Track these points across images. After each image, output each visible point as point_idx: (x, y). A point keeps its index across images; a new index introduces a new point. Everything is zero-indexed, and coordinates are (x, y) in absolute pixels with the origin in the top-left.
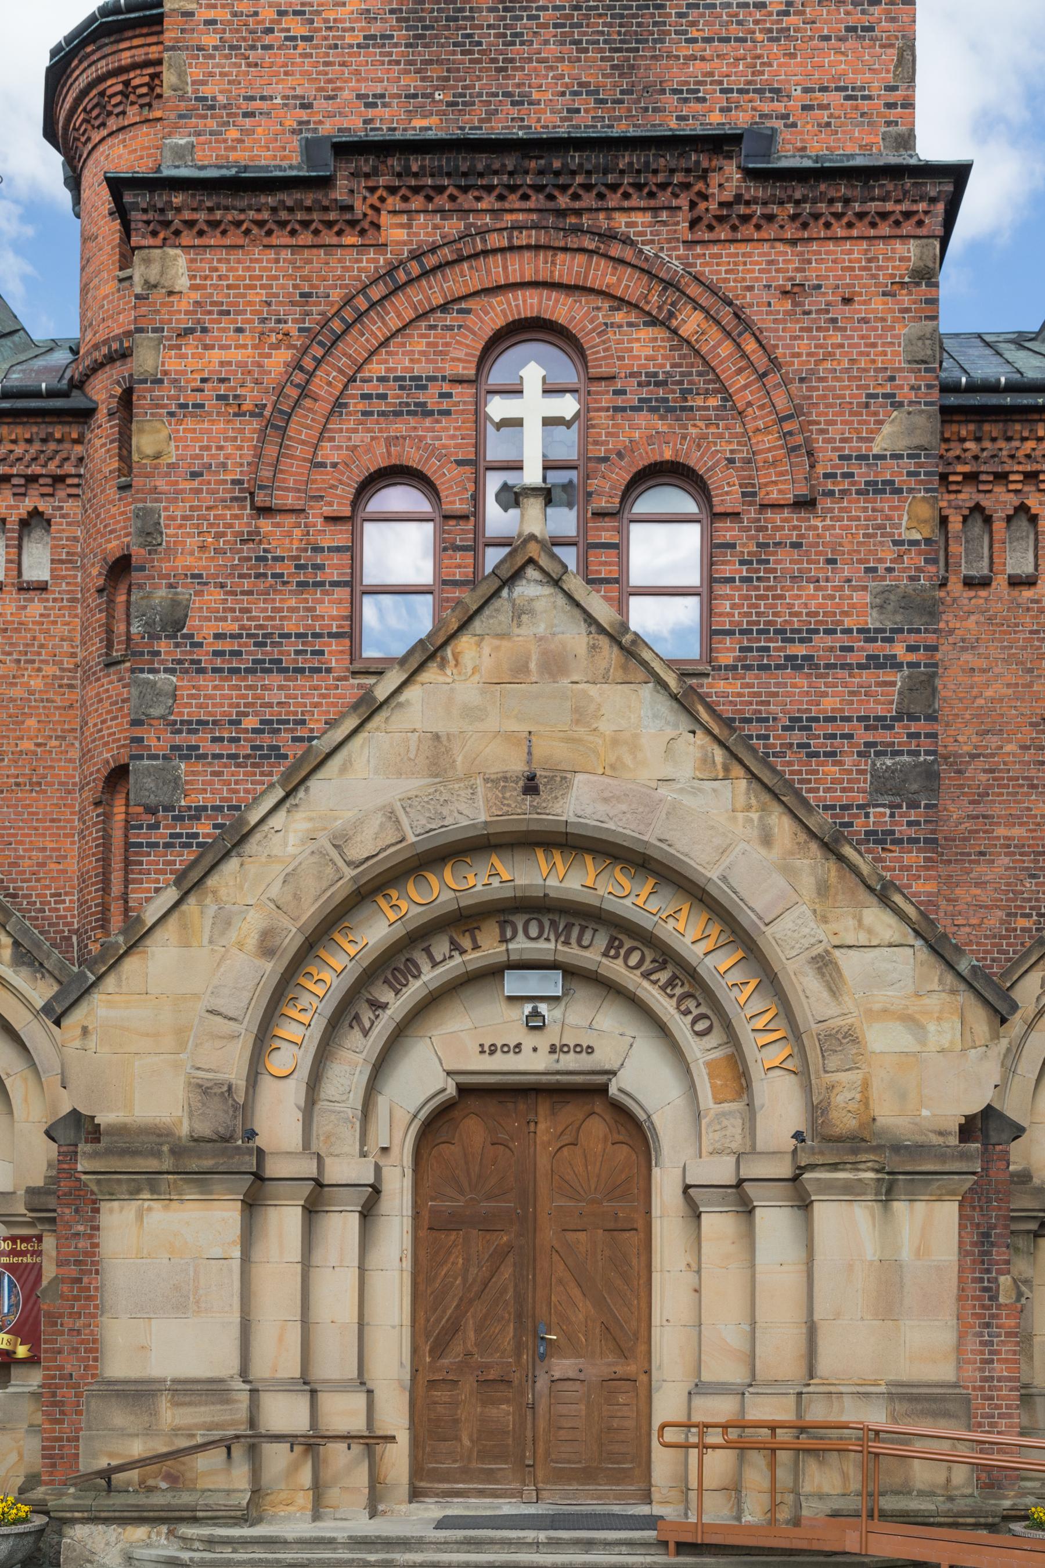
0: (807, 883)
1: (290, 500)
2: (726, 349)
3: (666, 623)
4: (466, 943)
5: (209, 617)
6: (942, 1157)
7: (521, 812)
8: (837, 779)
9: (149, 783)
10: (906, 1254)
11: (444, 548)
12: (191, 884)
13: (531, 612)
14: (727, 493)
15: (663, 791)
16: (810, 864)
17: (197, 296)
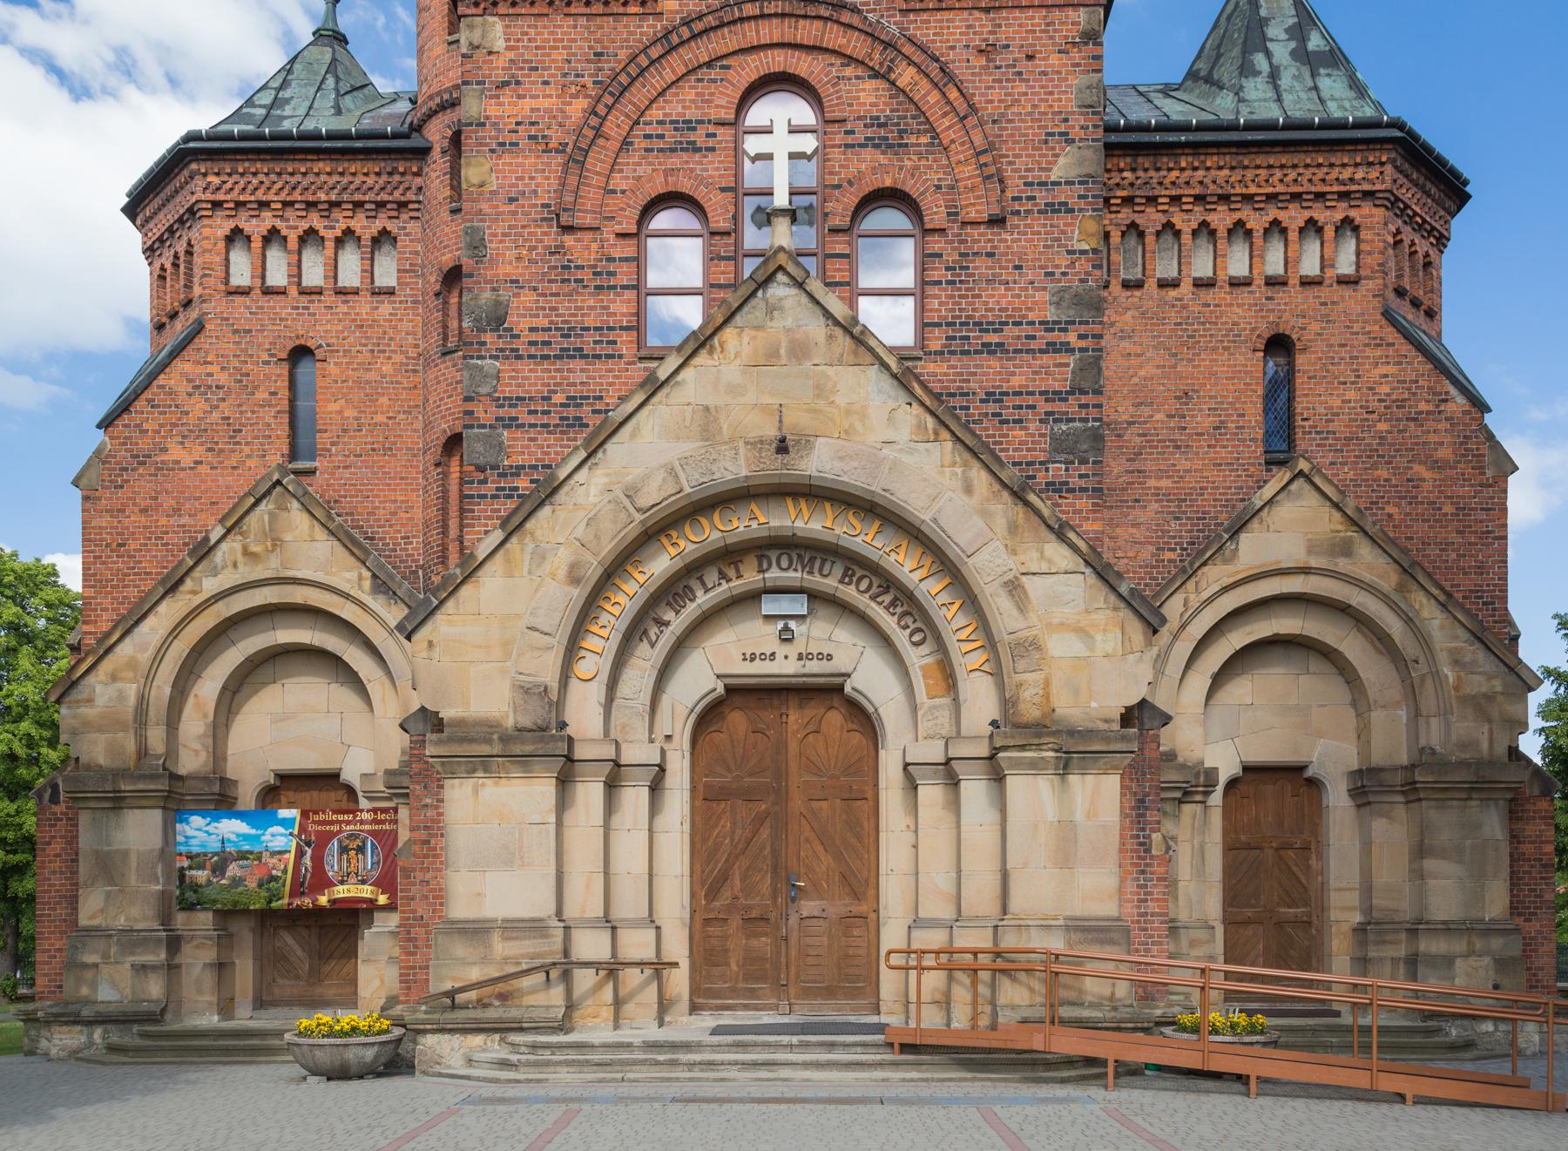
0: (1000, 523)
1: (588, 220)
2: (934, 97)
3: (892, 322)
4: (731, 573)
5: (525, 314)
6: (1107, 740)
7: (772, 468)
8: (1024, 441)
9: (479, 447)
10: (1079, 816)
11: (711, 258)
12: (513, 527)
13: (781, 309)
14: (936, 214)
15: (886, 451)
16: (1004, 509)
17: (511, 55)
